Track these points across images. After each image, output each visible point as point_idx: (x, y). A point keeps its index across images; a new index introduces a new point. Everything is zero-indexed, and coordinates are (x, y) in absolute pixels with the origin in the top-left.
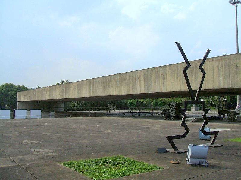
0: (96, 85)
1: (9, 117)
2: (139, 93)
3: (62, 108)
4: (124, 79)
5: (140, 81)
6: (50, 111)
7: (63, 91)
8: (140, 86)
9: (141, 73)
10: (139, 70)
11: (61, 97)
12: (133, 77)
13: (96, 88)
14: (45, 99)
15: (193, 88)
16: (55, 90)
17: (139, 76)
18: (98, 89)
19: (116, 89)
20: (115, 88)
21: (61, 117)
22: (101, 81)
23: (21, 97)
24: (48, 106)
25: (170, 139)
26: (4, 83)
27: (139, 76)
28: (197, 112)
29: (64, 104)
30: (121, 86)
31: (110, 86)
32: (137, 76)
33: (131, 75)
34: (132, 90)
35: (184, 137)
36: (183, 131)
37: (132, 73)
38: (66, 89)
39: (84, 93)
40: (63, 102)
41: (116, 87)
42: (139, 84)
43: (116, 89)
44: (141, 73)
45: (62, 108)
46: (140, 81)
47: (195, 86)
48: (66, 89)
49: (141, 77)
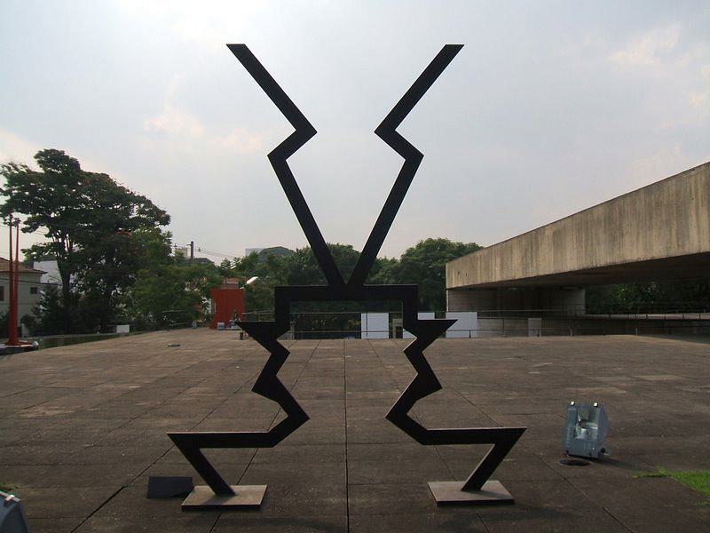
0: (594, 230)
1: (386, 335)
2: (695, 252)
3: (578, 303)
4: (657, 203)
5: (697, 209)
6: (532, 315)
7: (526, 255)
8: (698, 226)
9: (698, 177)
10: (693, 169)
11: (525, 268)
12: (678, 194)
13: (594, 242)
14: (479, 282)
15: (331, 237)
16: (512, 251)
17: (693, 193)
18: (598, 244)
19: (637, 239)
20: (635, 238)
21: (561, 335)
22: (602, 217)
23: (456, 277)
24: (529, 302)
25: (190, 445)
26: (425, 239)
27: (693, 193)
28: (394, 329)
29: (583, 293)
30: (650, 228)
31: (625, 232)
32: (688, 190)
33: (673, 187)
34: (678, 241)
35: (423, 443)
36: (269, 414)
37: (674, 181)
38: (532, 249)
39: (568, 257)
40: (580, 288)
41: (638, 234)
42: (694, 217)
43: (637, 239)
44: (698, 177)
45: (578, 303)
46: (697, 209)
47: (346, 228)
48: (532, 249)
49: (699, 195)
